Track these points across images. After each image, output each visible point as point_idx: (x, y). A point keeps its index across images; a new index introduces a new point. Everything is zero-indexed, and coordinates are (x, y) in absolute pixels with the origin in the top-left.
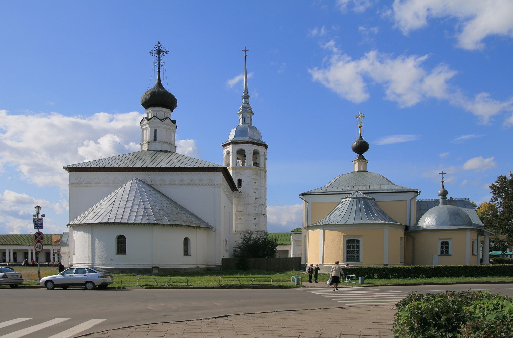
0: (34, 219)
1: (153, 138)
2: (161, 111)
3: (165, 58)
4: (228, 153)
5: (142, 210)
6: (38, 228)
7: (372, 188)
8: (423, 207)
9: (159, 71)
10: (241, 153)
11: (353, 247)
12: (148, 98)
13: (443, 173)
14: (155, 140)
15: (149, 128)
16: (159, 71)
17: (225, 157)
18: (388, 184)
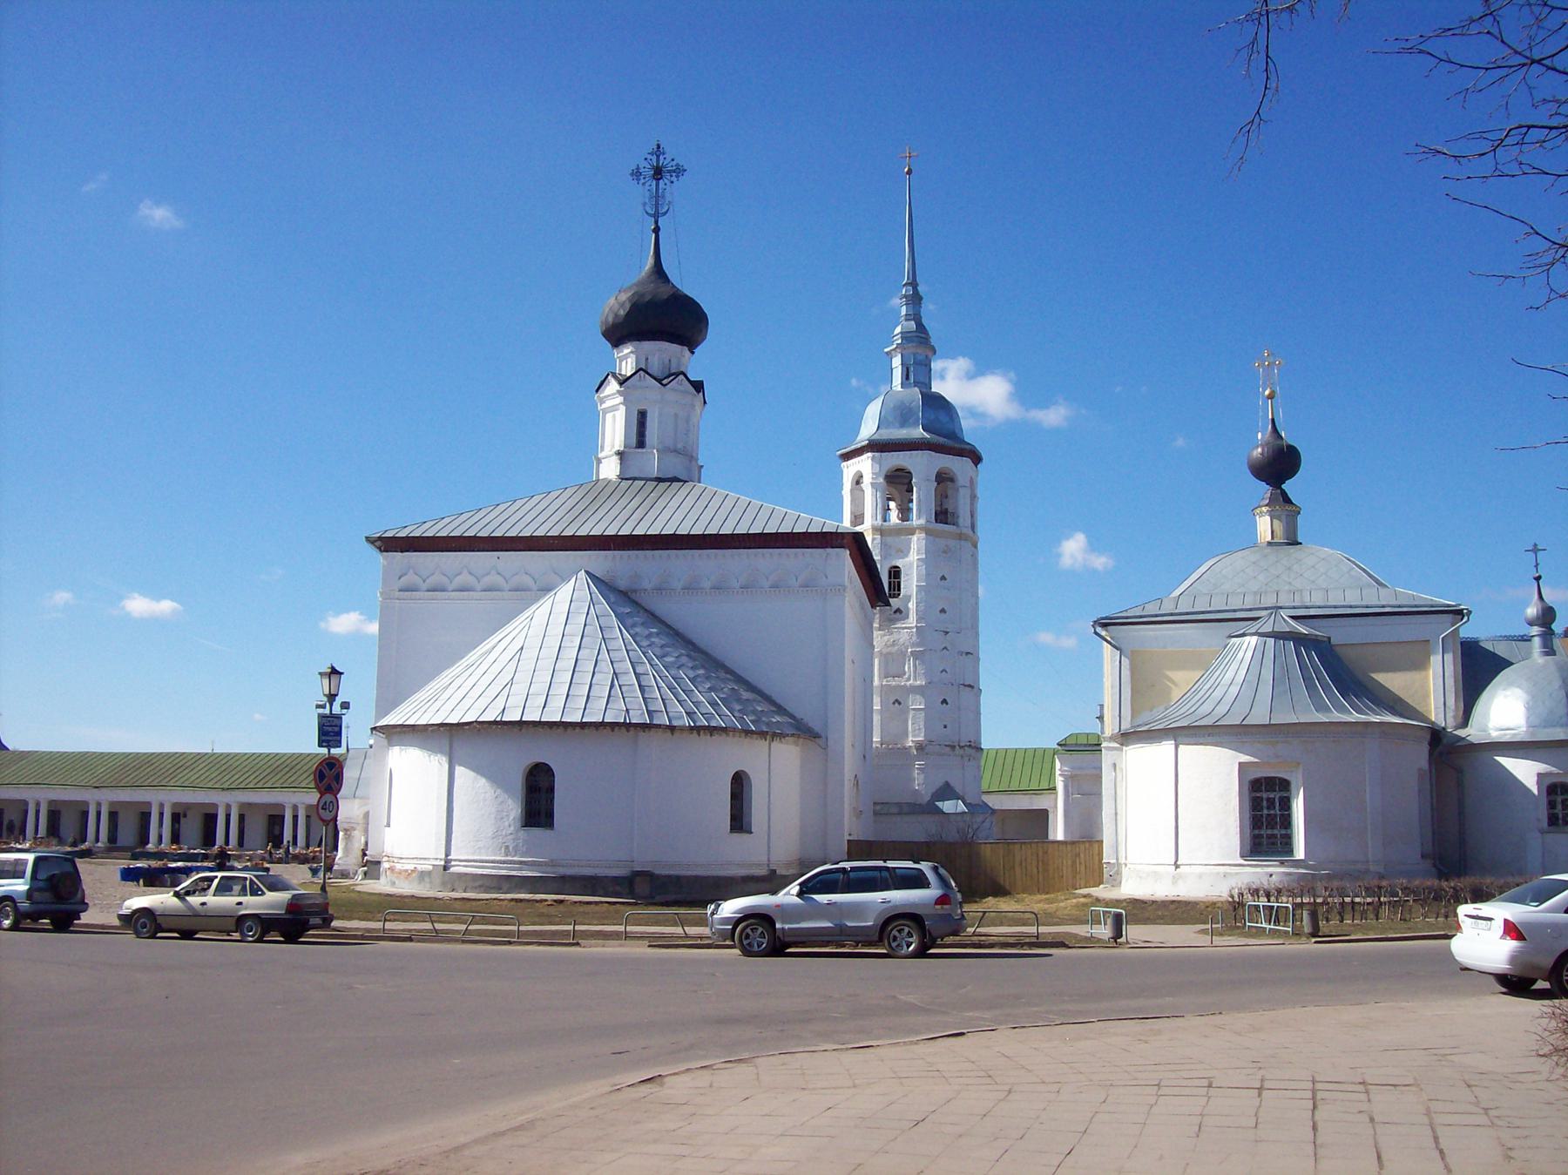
0: (321, 717)
1: (634, 441)
2: (662, 352)
3: (674, 190)
4: (858, 481)
5: (604, 678)
6: (329, 747)
7: (1317, 599)
8: (1479, 669)
9: (657, 230)
10: (898, 482)
11: (1271, 802)
12: (622, 313)
13: (1535, 550)
14: (641, 443)
15: (623, 408)
16: (657, 230)
17: (857, 496)
18: (1369, 585)
